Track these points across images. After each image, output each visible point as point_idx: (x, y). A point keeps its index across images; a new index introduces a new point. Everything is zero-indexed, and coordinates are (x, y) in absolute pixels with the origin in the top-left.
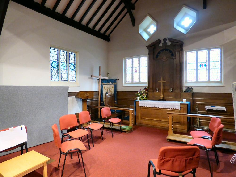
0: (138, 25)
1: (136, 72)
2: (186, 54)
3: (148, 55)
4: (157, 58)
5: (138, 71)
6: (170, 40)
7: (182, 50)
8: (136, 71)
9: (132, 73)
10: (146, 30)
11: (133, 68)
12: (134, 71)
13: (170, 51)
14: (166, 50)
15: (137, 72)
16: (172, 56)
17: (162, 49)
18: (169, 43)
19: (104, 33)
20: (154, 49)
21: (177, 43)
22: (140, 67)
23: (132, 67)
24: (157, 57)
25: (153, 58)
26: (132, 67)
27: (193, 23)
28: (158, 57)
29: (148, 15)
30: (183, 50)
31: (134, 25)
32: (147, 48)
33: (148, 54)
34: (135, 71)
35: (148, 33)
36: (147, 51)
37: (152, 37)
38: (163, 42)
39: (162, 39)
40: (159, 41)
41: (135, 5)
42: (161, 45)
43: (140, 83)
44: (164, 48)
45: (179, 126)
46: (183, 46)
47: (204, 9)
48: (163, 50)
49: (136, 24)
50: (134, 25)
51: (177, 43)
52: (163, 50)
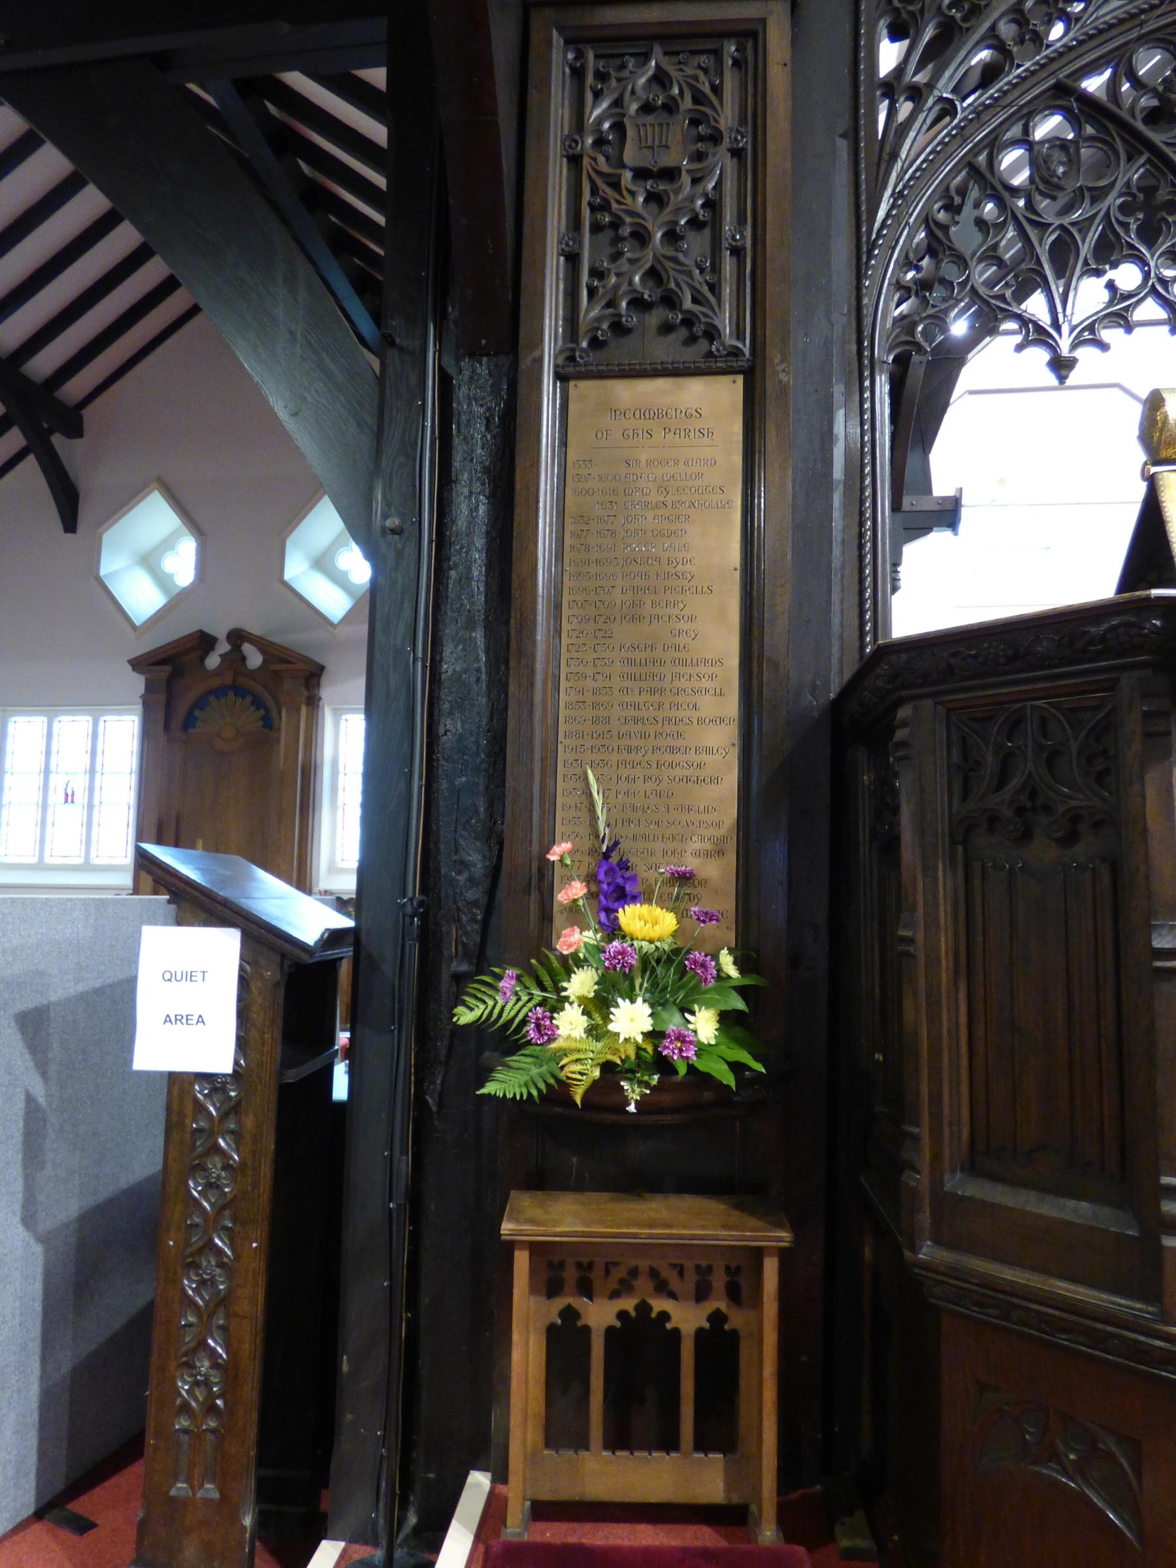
0: (100, 524)
1: (68, 798)
2: (337, 726)
3: (139, 708)
4: (191, 730)
5: (81, 797)
6: (261, 644)
7: (313, 702)
8: (70, 794)
9: (44, 806)
10: (149, 561)
11: (52, 777)
12: (55, 797)
13: (258, 703)
14: (240, 692)
15: (72, 802)
16: (264, 727)
17: (217, 682)
18: (254, 659)
19: (39, 143)
20: (170, 680)
21: (291, 663)
22: (92, 771)
23: (47, 772)
24: (189, 722)
25: (167, 727)
26: (47, 772)
27: (66, 710)
28: (194, 726)
29: (155, 484)
30: (321, 703)
31: (70, 524)
32: (130, 668)
33: (141, 701)
34: (63, 796)
35: (162, 580)
36: (138, 683)
37: (178, 601)
38: (224, 647)
39: (220, 630)
40: (205, 642)
41: (88, 413)
42: (213, 661)
43: (87, 867)
44: (228, 681)
45: (557, 1223)
46: (324, 680)
47: (129, 662)
48: (219, 692)
49: (86, 514)
50: (70, 524)
51: (291, 663)
52: (219, 692)
